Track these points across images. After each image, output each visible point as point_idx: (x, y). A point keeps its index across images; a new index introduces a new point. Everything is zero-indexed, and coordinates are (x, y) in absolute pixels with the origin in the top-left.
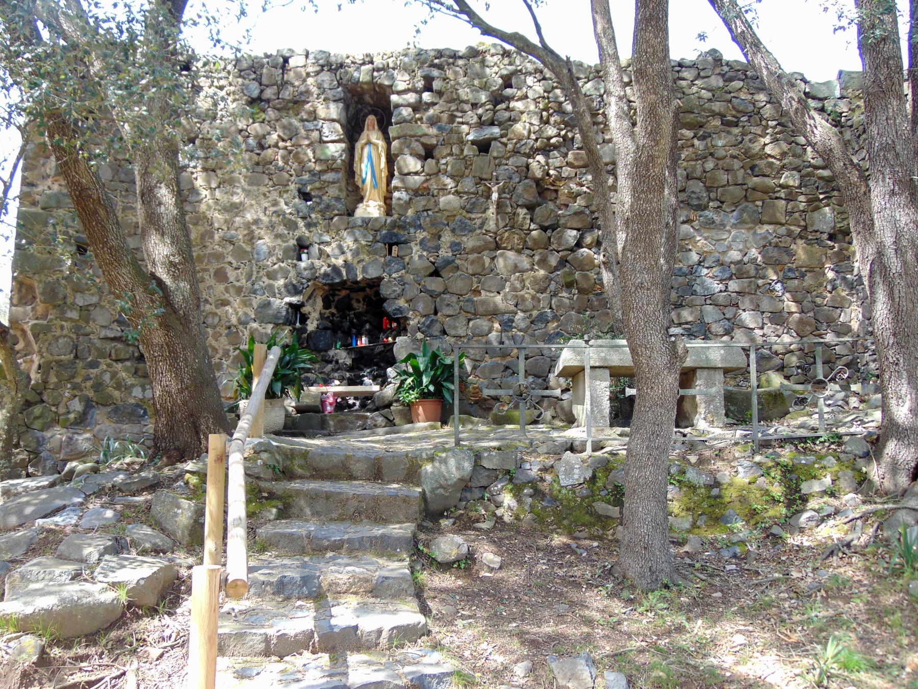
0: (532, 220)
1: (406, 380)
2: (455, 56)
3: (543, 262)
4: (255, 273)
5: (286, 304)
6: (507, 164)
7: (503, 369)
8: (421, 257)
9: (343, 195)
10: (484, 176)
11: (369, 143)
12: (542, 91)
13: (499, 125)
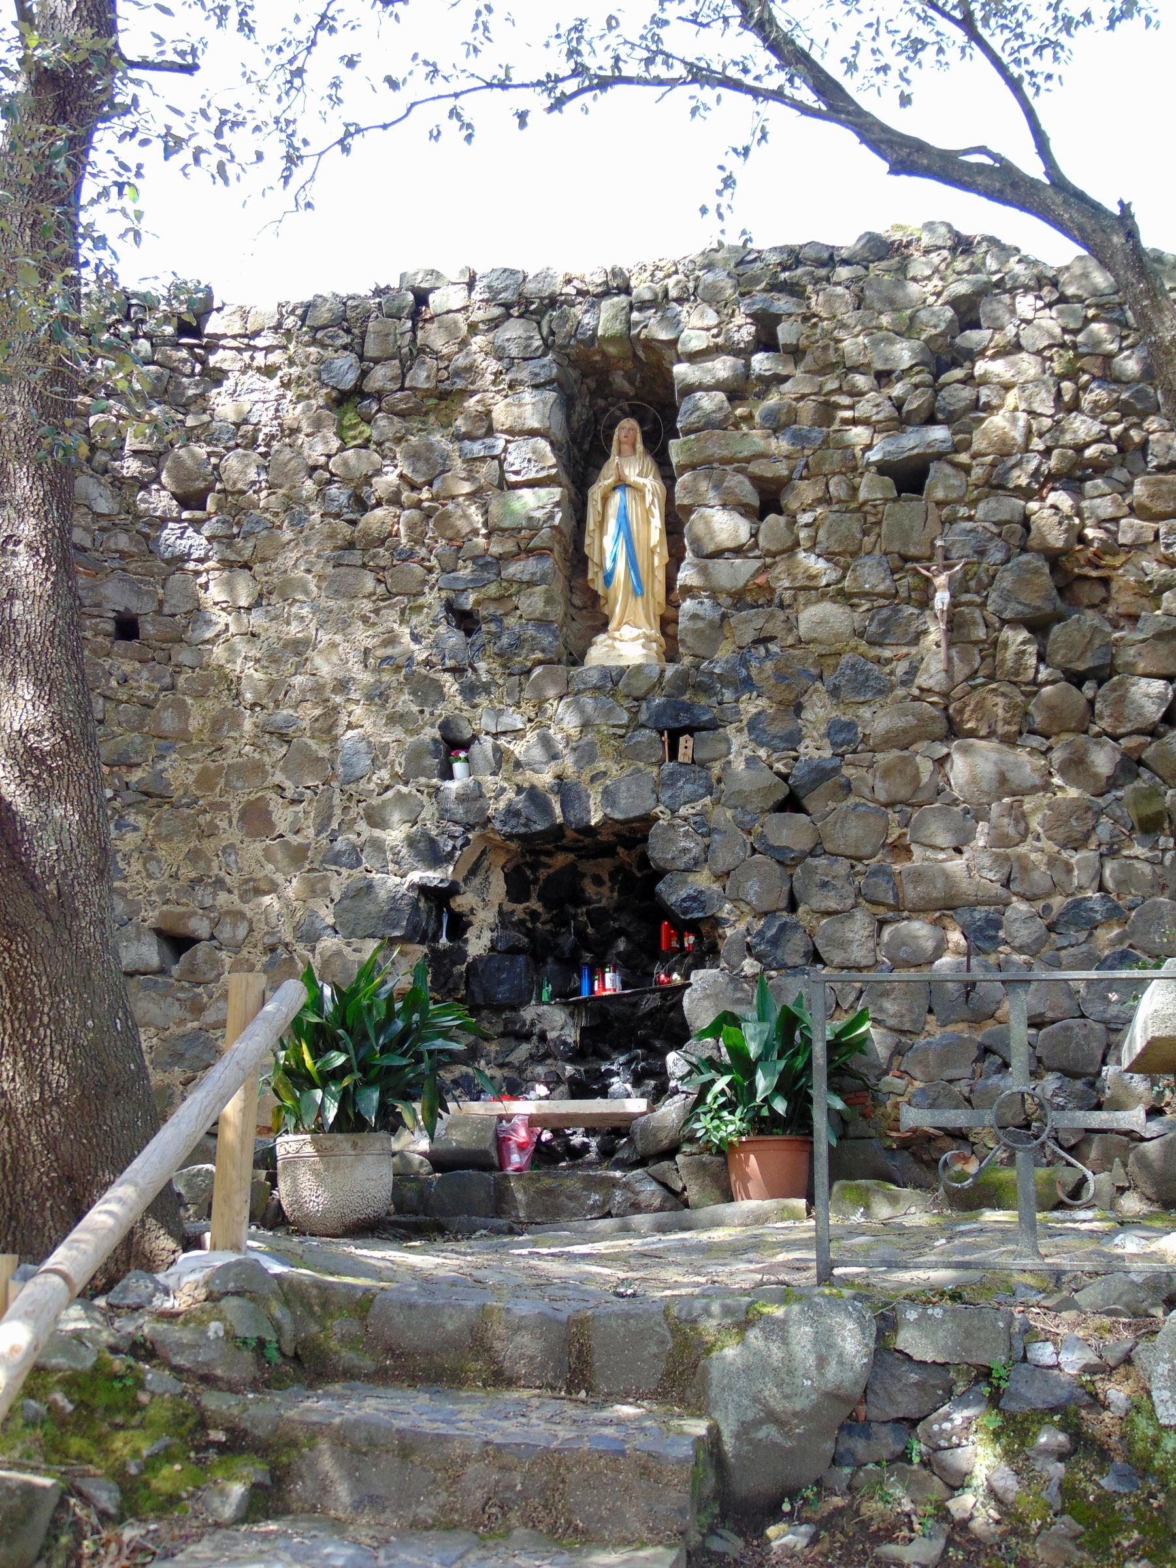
0: (1041, 658)
1: (712, 1082)
2: (829, 259)
3: (1076, 766)
4: (338, 811)
5: (412, 886)
6: (970, 518)
7: (975, 1053)
8: (751, 761)
9: (557, 612)
10: (913, 551)
11: (621, 484)
12: (1057, 331)
13: (947, 422)
